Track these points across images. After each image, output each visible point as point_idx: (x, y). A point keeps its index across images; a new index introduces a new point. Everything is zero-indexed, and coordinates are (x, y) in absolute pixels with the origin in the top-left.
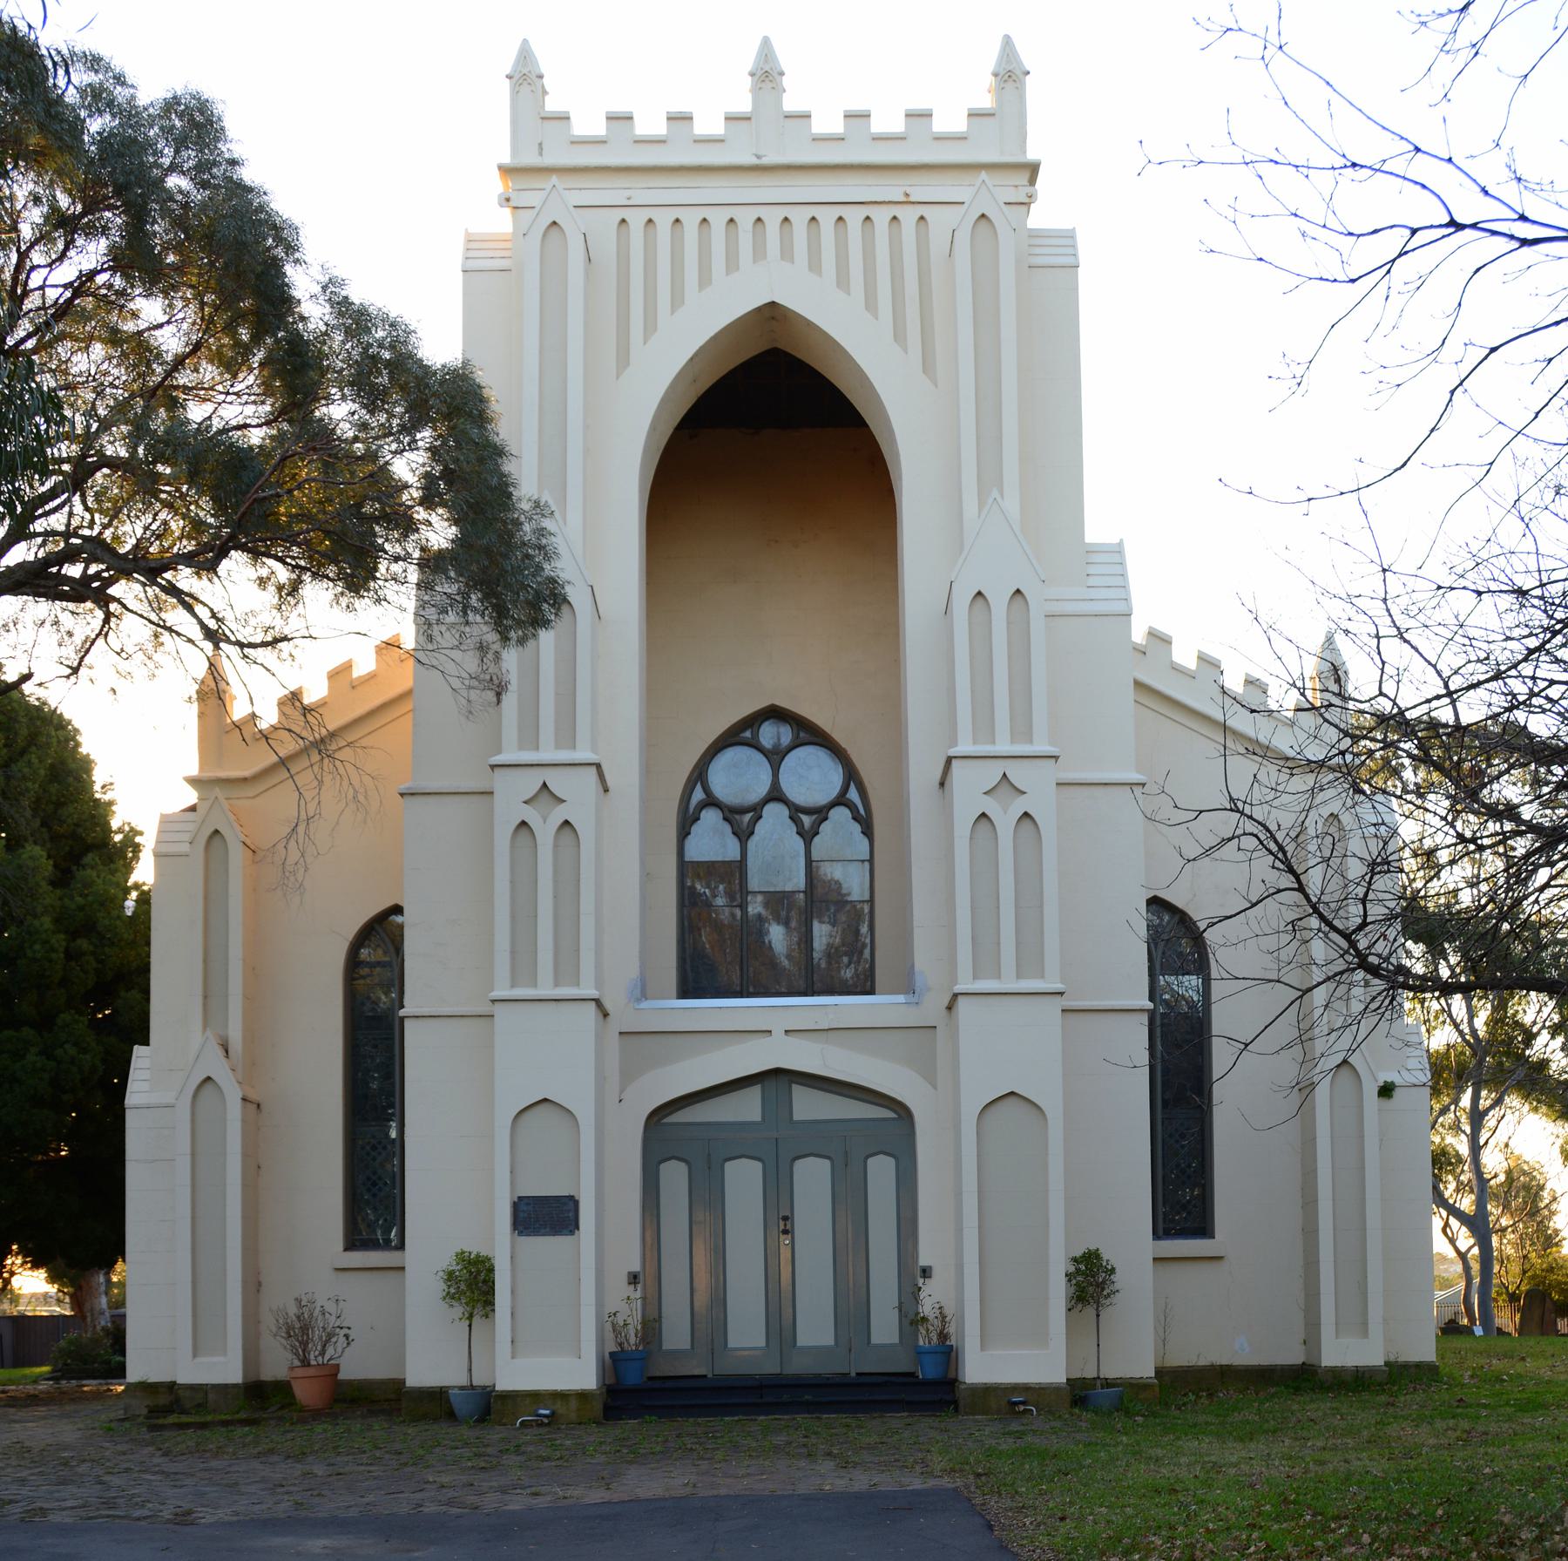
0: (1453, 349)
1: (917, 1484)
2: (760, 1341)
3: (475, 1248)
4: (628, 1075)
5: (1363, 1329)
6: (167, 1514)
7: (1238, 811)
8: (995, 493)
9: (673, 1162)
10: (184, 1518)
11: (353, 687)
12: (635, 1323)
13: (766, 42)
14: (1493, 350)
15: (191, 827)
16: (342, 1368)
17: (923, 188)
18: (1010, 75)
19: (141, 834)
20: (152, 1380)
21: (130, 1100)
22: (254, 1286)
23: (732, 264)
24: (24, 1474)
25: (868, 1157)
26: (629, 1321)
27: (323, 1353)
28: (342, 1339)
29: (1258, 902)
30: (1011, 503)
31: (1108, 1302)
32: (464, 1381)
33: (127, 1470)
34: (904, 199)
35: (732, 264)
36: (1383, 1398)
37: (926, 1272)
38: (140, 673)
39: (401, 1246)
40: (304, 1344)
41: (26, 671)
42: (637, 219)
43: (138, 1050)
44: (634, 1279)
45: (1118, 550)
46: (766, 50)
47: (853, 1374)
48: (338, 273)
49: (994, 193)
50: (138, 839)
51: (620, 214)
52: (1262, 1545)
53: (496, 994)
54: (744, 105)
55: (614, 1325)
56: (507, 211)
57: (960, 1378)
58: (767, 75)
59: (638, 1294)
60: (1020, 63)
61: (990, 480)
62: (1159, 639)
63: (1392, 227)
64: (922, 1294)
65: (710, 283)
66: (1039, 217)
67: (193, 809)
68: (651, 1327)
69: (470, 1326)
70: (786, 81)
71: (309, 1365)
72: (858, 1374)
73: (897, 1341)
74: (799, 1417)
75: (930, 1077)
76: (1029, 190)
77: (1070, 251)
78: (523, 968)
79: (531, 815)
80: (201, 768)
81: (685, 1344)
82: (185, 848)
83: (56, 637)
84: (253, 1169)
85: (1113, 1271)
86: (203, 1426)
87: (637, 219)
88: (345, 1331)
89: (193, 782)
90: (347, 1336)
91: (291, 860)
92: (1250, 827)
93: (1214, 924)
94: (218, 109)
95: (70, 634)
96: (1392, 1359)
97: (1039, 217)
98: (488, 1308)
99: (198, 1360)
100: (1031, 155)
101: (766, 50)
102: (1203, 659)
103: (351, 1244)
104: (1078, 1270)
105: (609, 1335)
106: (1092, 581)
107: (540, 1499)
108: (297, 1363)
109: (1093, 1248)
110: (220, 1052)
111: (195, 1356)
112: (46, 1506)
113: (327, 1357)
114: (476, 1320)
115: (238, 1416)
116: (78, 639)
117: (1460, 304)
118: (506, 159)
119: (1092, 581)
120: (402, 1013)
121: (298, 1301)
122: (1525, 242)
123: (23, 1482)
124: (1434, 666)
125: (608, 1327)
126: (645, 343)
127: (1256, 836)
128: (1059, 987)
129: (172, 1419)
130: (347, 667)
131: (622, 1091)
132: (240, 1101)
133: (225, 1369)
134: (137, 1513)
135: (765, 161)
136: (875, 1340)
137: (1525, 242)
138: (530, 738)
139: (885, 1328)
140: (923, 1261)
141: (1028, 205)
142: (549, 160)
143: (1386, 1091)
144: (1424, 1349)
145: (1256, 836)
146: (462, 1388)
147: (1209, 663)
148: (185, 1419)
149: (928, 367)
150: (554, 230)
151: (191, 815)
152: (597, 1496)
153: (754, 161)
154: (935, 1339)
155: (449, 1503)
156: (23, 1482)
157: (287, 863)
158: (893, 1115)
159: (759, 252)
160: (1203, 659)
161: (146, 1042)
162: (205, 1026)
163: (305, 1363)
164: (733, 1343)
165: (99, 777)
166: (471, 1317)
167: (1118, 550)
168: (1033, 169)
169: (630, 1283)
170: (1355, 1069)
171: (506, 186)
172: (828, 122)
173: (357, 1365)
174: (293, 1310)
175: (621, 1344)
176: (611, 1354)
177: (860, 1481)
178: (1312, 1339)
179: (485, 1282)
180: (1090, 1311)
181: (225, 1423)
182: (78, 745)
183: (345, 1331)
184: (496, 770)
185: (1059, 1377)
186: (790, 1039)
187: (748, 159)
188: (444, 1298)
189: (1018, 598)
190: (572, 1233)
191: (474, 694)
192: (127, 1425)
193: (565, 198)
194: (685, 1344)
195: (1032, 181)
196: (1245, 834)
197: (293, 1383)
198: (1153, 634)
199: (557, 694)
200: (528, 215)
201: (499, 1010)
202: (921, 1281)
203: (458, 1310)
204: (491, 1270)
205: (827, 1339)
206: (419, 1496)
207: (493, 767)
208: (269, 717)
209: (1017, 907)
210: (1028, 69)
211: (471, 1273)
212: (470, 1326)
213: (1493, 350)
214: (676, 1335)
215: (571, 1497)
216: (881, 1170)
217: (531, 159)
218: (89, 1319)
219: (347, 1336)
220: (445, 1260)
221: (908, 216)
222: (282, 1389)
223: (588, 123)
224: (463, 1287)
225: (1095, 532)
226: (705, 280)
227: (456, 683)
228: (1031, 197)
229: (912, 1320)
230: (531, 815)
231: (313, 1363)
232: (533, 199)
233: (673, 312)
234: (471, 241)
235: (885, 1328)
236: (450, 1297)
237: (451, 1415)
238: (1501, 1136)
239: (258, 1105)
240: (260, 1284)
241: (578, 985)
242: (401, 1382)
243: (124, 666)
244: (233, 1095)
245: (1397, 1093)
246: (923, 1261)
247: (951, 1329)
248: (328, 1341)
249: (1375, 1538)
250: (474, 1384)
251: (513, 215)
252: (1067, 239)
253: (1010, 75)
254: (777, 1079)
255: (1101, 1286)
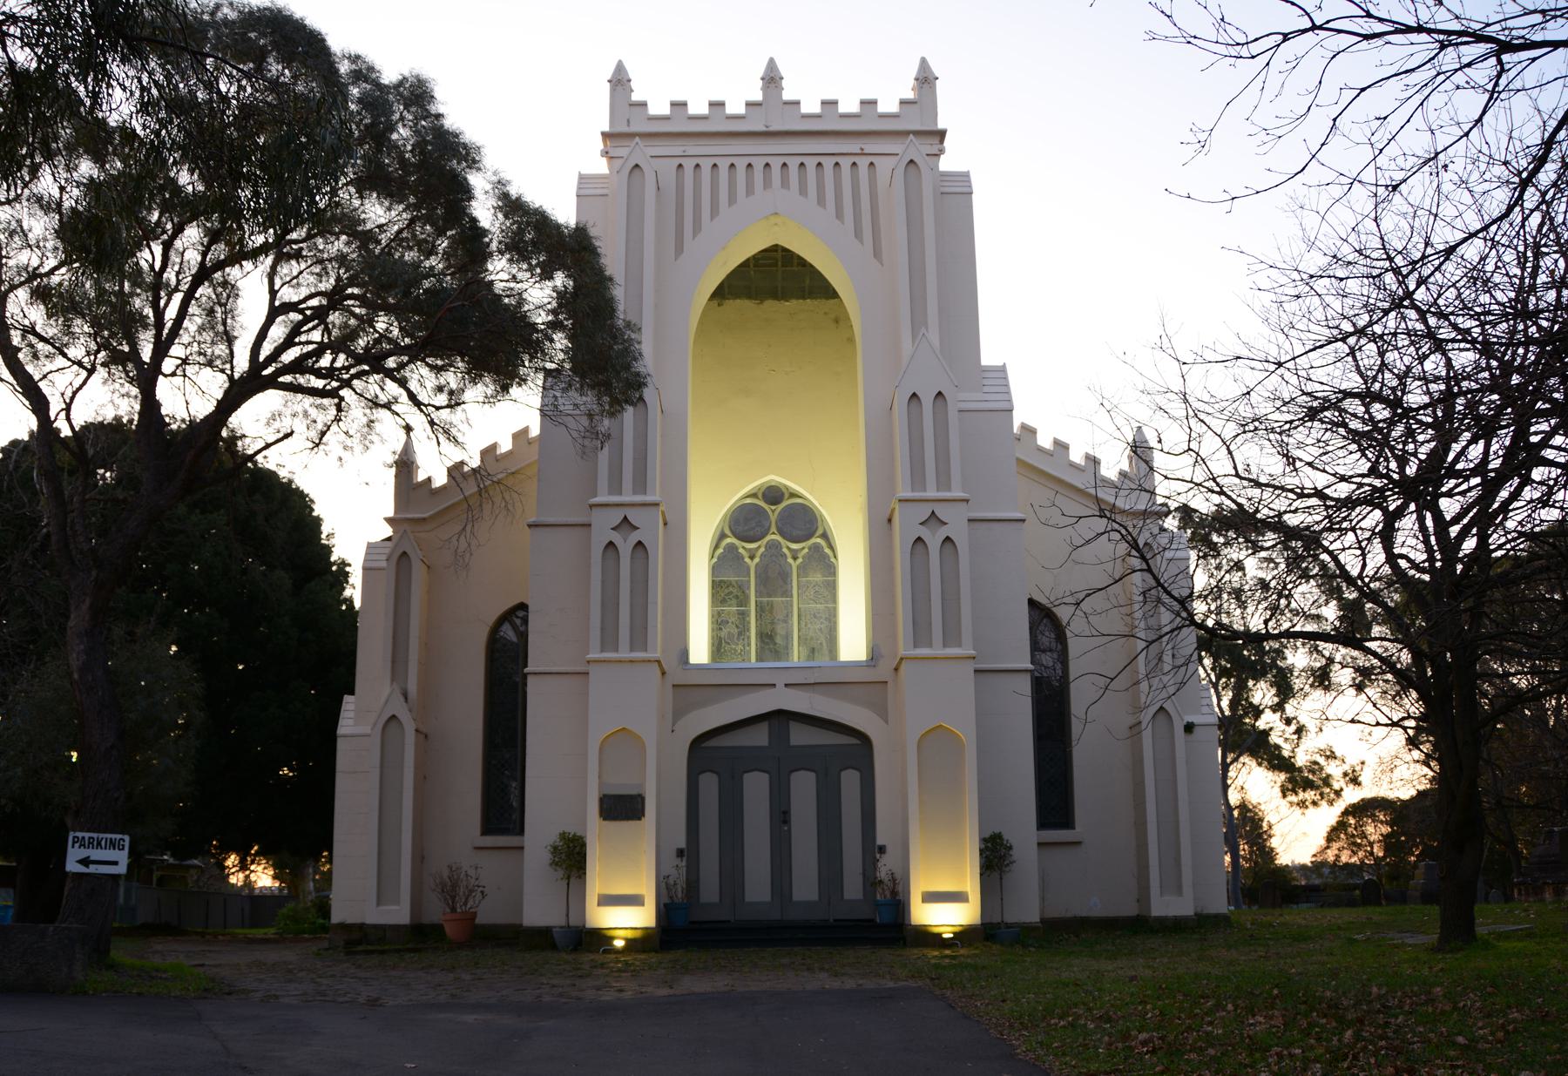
0: (1328, 94)
1: (891, 984)
2: (767, 897)
3: (572, 830)
4: (678, 714)
5: (1179, 890)
6: (361, 1000)
7: (1106, 517)
8: (923, 330)
9: (708, 774)
10: (373, 1003)
11: (497, 461)
12: (682, 883)
13: (772, 61)
14: (1363, 90)
15: (387, 551)
16: (479, 915)
17: (872, 146)
18: (925, 79)
19: (349, 565)
20: (349, 921)
21: (341, 731)
22: (419, 858)
23: (750, 190)
24: (262, 977)
25: (841, 770)
26: (678, 881)
27: (465, 904)
28: (479, 894)
29: (1120, 579)
30: (934, 336)
31: (1007, 869)
32: (563, 923)
33: (332, 976)
34: (860, 152)
35: (750, 190)
36: (1196, 936)
37: (882, 849)
38: (358, 448)
39: (521, 832)
40: (453, 898)
41: (289, 431)
42: (689, 164)
43: (347, 698)
44: (680, 853)
45: (1002, 370)
46: (772, 64)
47: (831, 920)
48: (505, 176)
49: (917, 149)
50: (347, 569)
51: (677, 161)
52: (1157, 1012)
53: (591, 656)
54: (758, 96)
55: (667, 884)
56: (604, 160)
57: (906, 922)
58: (772, 79)
59: (684, 863)
60: (932, 73)
61: (918, 322)
62: (1029, 431)
63: (1267, 35)
64: (879, 864)
65: (735, 202)
66: (946, 164)
67: (389, 539)
68: (693, 884)
69: (568, 884)
70: (784, 83)
71: (456, 911)
72: (835, 920)
73: (862, 897)
74: (796, 949)
75: (883, 714)
76: (939, 146)
77: (967, 184)
78: (609, 639)
79: (616, 537)
80: (395, 512)
81: (715, 898)
82: (384, 564)
83: (305, 422)
84: (422, 779)
85: (1010, 848)
86: (382, 952)
87: (689, 164)
88: (481, 889)
89: (389, 520)
90: (482, 892)
91: (461, 549)
92: (1116, 526)
93: (1090, 595)
94: (431, 85)
95: (315, 422)
96: (1199, 910)
97: (946, 164)
98: (581, 872)
99: (381, 908)
100: (941, 126)
101: (772, 64)
102: (1057, 442)
103: (487, 830)
104: (987, 847)
105: (664, 891)
106: (986, 389)
107: (624, 994)
108: (448, 910)
109: (997, 831)
110: (402, 699)
111: (379, 904)
112: (278, 993)
113: (469, 906)
114: (572, 880)
115: (409, 946)
116: (320, 426)
117: (1320, 82)
118: (607, 129)
119: (986, 389)
120: (526, 670)
121: (450, 867)
122: (1367, 37)
123: (261, 981)
124: (1219, 436)
125: (663, 885)
126: (694, 238)
127: (1119, 532)
128: (972, 652)
129: (360, 948)
130: (494, 447)
131: (673, 725)
132: (413, 732)
133: (398, 913)
134: (341, 999)
135: (772, 128)
136: (847, 896)
137: (1367, 37)
138: (616, 487)
139: (853, 888)
140: (879, 842)
141: (938, 156)
142: (634, 128)
143: (1189, 728)
144: (1219, 903)
145: (1119, 532)
146: (562, 927)
147: (1061, 446)
148: (370, 947)
149: (877, 253)
150: (637, 171)
151: (388, 544)
152: (664, 992)
153: (764, 129)
154: (888, 896)
155: (561, 995)
156: (261, 981)
157: (459, 551)
158: (858, 742)
159: (767, 183)
160: (1057, 442)
161: (352, 693)
162: (393, 680)
163: (453, 910)
164: (748, 898)
165: (325, 529)
166: (569, 878)
167: (1002, 370)
168: (941, 135)
169: (678, 856)
170: (1169, 714)
171: (605, 145)
172: (811, 106)
173: (489, 913)
174: (446, 873)
175: (671, 898)
176: (665, 905)
177: (850, 984)
178: (1144, 897)
179: (578, 853)
180: (996, 875)
181: (398, 951)
182: (313, 510)
183: (481, 889)
184: (594, 509)
185: (1192, 913)
186: (790, 691)
187: (761, 128)
188: (551, 864)
189: (940, 398)
190: (640, 819)
191: (587, 442)
192: (331, 951)
193: (642, 153)
194: (715, 898)
195: (942, 141)
196: (1112, 530)
197: (445, 925)
198: (1024, 427)
199: (634, 459)
200: (618, 163)
201: (592, 669)
202: (878, 856)
203: (561, 873)
204: (584, 845)
205: (813, 896)
206: (538, 991)
207: (591, 506)
208: (440, 479)
209: (943, 599)
210: (937, 75)
211: (569, 847)
212: (568, 884)
213: (1363, 90)
214: (710, 891)
215: (646, 992)
216: (850, 781)
217: (624, 129)
218: (301, 897)
219: (482, 892)
220: (552, 837)
221: (863, 163)
222: (437, 929)
223: (659, 107)
224: (563, 856)
225: (988, 358)
226: (732, 200)
227: (575, 434)
228: (942, 151)
229: (871, 881)
230: (616, 537)
231: (459, 910)
232: (623, 152)
233: (712, 220)
234: (583, 179)
235: (853, 888)
236: (554, 864)
237: (553, 947)
238: (1239, 783)
239: (426, 736)
240: (423, 858)
241: (646, 650)
242: (521, 925)
243: (349, 442)
244: (409, 727)
245: (1197, 730)
246: (879, 842)
247: (900, 888)
248: (469, 896)
249: (1236, 1007)
250: (571, 924)
251: (609, 164)
252: (965, 177)
253: (925, 79)
254: (780, 718)
255: (1002, 858)
